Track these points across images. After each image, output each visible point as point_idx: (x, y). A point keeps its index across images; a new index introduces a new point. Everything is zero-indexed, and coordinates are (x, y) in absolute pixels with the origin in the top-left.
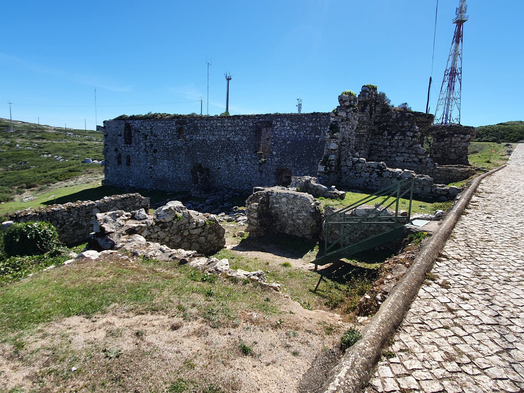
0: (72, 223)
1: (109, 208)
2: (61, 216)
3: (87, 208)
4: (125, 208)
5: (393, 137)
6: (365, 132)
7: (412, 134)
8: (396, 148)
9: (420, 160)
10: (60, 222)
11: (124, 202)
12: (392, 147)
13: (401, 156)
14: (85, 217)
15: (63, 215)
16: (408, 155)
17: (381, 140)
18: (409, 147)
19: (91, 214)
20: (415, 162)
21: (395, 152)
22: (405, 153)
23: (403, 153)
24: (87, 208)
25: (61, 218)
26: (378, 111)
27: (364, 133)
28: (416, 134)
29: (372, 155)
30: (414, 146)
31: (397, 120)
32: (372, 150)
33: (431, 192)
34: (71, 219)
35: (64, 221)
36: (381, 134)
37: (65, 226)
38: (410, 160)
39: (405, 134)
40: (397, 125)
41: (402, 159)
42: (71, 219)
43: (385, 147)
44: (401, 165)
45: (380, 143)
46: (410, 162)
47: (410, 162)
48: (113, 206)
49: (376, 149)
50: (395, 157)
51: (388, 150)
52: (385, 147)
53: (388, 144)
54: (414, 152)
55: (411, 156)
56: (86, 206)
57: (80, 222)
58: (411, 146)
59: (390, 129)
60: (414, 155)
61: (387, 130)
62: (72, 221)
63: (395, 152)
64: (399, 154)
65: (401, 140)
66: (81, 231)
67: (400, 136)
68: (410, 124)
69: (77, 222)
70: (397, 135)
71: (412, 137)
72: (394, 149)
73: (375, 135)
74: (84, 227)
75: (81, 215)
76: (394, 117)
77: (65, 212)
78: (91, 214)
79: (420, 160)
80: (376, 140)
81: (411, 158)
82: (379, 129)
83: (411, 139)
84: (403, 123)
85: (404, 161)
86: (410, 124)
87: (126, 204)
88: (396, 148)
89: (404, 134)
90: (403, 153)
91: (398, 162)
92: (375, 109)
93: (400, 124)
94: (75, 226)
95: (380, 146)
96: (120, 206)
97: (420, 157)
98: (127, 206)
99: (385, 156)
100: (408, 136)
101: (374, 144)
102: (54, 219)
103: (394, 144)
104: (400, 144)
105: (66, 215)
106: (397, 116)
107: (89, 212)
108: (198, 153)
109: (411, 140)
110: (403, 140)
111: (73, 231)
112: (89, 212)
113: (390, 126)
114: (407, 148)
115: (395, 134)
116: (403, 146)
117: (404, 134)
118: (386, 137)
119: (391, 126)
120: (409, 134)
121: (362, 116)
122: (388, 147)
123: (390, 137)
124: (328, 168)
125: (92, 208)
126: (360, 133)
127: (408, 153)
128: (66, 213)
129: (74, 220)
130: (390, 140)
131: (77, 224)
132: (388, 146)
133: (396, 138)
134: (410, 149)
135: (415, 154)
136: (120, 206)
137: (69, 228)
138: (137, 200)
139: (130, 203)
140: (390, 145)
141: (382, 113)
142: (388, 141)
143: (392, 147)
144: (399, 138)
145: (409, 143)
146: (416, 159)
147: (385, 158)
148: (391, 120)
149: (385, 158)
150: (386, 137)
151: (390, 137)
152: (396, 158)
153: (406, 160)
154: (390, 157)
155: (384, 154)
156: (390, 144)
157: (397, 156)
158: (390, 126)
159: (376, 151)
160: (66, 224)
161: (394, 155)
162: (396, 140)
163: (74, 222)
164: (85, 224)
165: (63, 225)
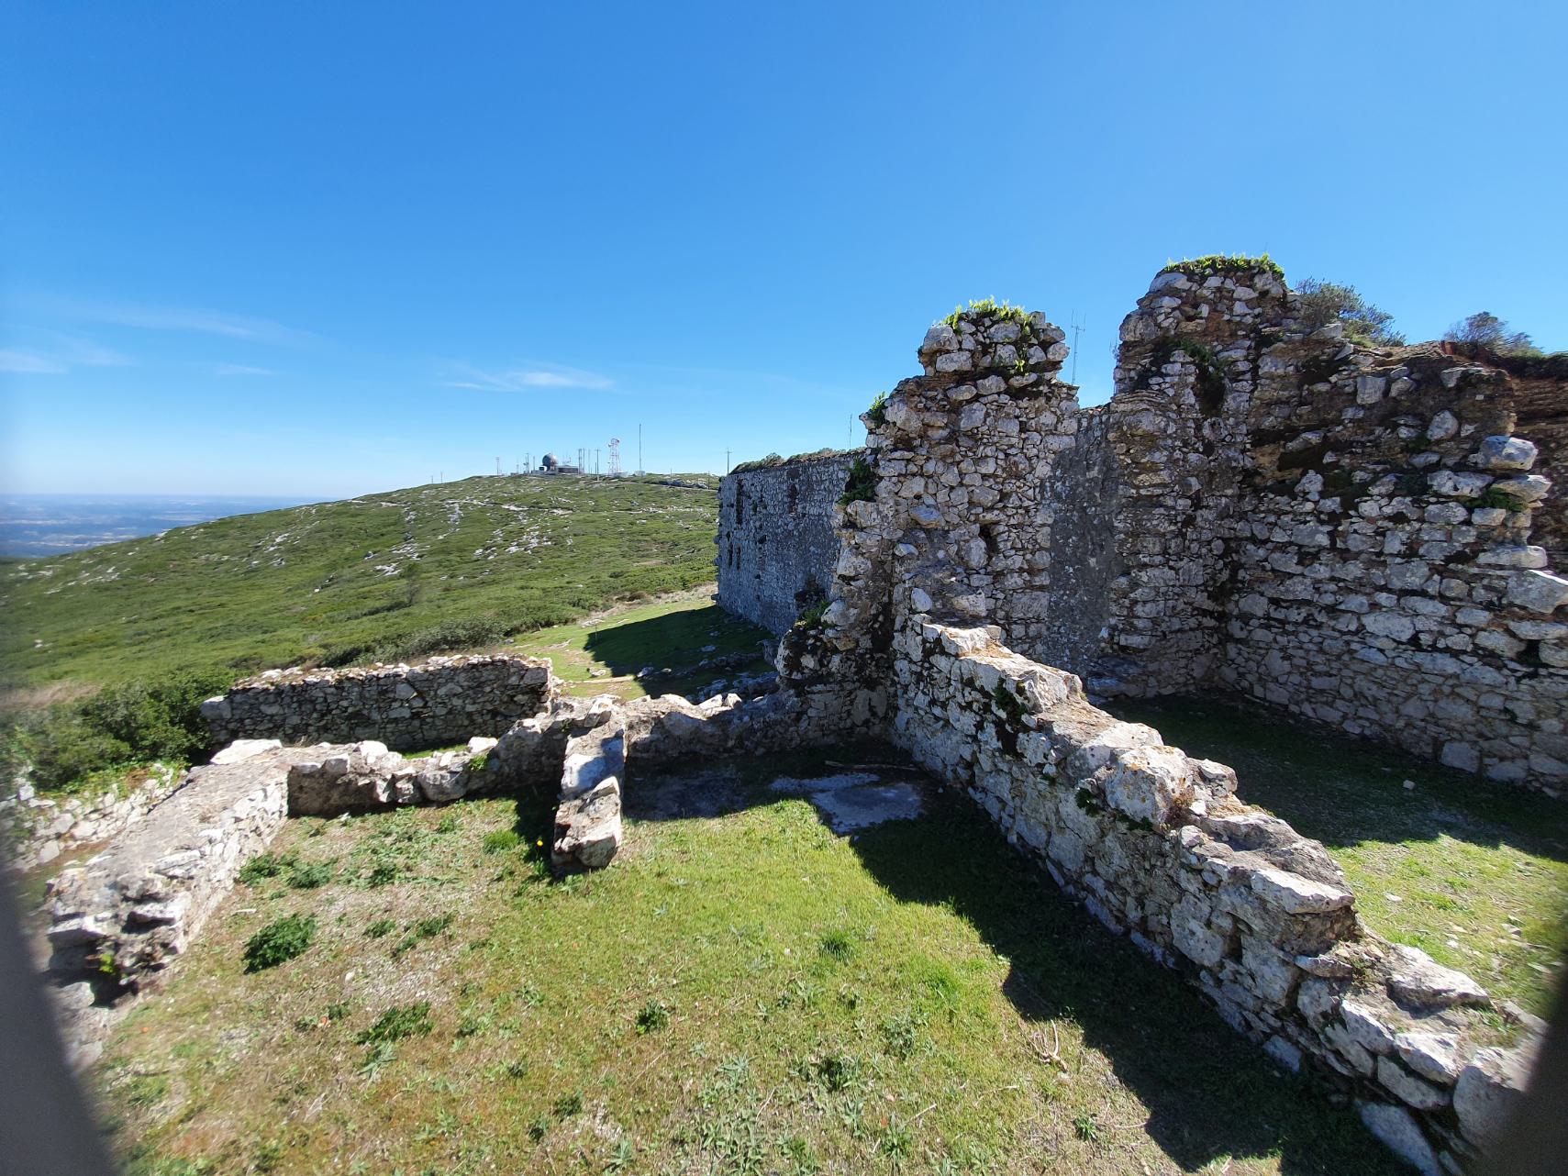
0: (345, 712)
1: (435, 685)
2: (322, 694)
3: (381, 682)
4: (478, 686)
5: (1350, 505)
6: (1164, 485)
7: (1470, 486)
8: (1370, 564)
9: (1530, 651)
10: (318, 707)
11: (477, 674)
12: (1345, 555)
13: (1402, 611)
14: (377, 701)
15: (326, 694)
16: (1443, 610)
17: (1286, 518)
18: (1448, 560)
19: (392, 695)
20: (1490, 657)
21: (1358, 587)
22: (1422, 593)
23: (1413, 593)
24: (381, 682)
25: (322, 699)
26: (1272, 378)
27: (1158, 491)
28: (1509, 486)
29: (1239, 591)
30: (1483, 558)
31: (1388, 413)
32: (1242, 566)
33: (1291, 1010)
34: (345, 703)
35: (328, 706)
36: (1286, 489)
37: (329, 717)
38: (1458, 641)
39: (1426, 488)
40: (1387, 435)
41: (1402, 628)
42: (345, 703)
43: (1307, 557)
44: (1399, 662)
45: (1279, 537)
46: (1455, 654)
47: (1455, 654)
48: (447, 682)
49: (1259, 564)
50: (1358, 615)
51: (1322, 571)
52: (1307, 557)
53: (1323, 540)
54: (1480, 594)
55: (1460, 619)
56: (378, 679)
57: (365, 712)
58: (1460, 557)
59: (1346, 461)
60: (1482, 617)
61: (1321, 469)
62: (347, 708)
63: (1358, 587)
64: (1382, 598)
65: (1399, 518)
66: (367, 730)
67: (1391, 496)
68: (1468, 429)
69: (360, 710)
70: (1374, 490)
71: (1471, 505)
72: (1354, 570)
73: (1257, 491)
74: (375, 723)
75: (367, 695)
76: (1370, 393)
77: (330, 686)
78: (392, 695)
79: (1530, 651)
80: (1261, 521)
81: (1460, 627)
82: (1285, 462)
83: (1461, 513)
84: (1425, 423)
85: (1414, 641)
86: (1468, 429)
87: (482, 679)
88: (1370, 564)
89: (1415, 486)
90: (1413, 593)
91: (1378, 643)
92: (1255, 370)
93: (1404, 433)
94: (354, 718)
95: (1282, 548)
96: (466, 683)
97: (1527, 630)
98: (484, 682)
99: (1308, 603)
100: (1443, 499)
101: (1253, 539)
102: (306, 699)
103: (1354, 543)
104: (1394, 545)
105: (332, 694)
106: (1386, 393)
107: (386, 691)
108: (812, 548)
109: (1468, 522)
110: (1408, 521)
111: (351, 729)
112: (386, 691)
113: (1340, 447)
114: (1434, 569)
115: (1363, 490)
116: (1411, 552)
117: (1415, 486)
118: (1309, 506)
119: (1350, 444)
120: (1447, 488)
121: (1133, 413)
122: (1324, 557)
123: (1332, 504)
124: (808, 662)
125: (395, 683)
126: (1138, 488)
127: (1443, 598)
128: (333, 689)
129: (351, 705)
130: (1334, 518)
131: (357, 714)
132: (1321, 549)
133: (1368, 508)
134: (1455, 575)
135: (1488, 606)
136: (466, 683)
137: (338, 721)
138: (512, 670)
139: (492, 677)
140: (1333, 548)
141: (1300, 387)
142: (1322, 522)
143: (1345, 555)
144: (1388, 510)
145: (1449, 538)
146: (1495, 641)
147: (1304, 612)
148: (1349, 413)
149: (1304, 612)
150: (1309, 506)
151: (1332, 504)
152: (1368, 621)
153: (1425, 639)
154: (1332, 610)
155: (1301, 589)
156: (1333, 542)
157: (1375, 606)
158: (1340, 447)
159: (1259, 573)
160: (334, 712)
161: (1356, 602)
162: (1371, 520)
163: (350, 710)
164: (376, 716)
165: (325, 715)
